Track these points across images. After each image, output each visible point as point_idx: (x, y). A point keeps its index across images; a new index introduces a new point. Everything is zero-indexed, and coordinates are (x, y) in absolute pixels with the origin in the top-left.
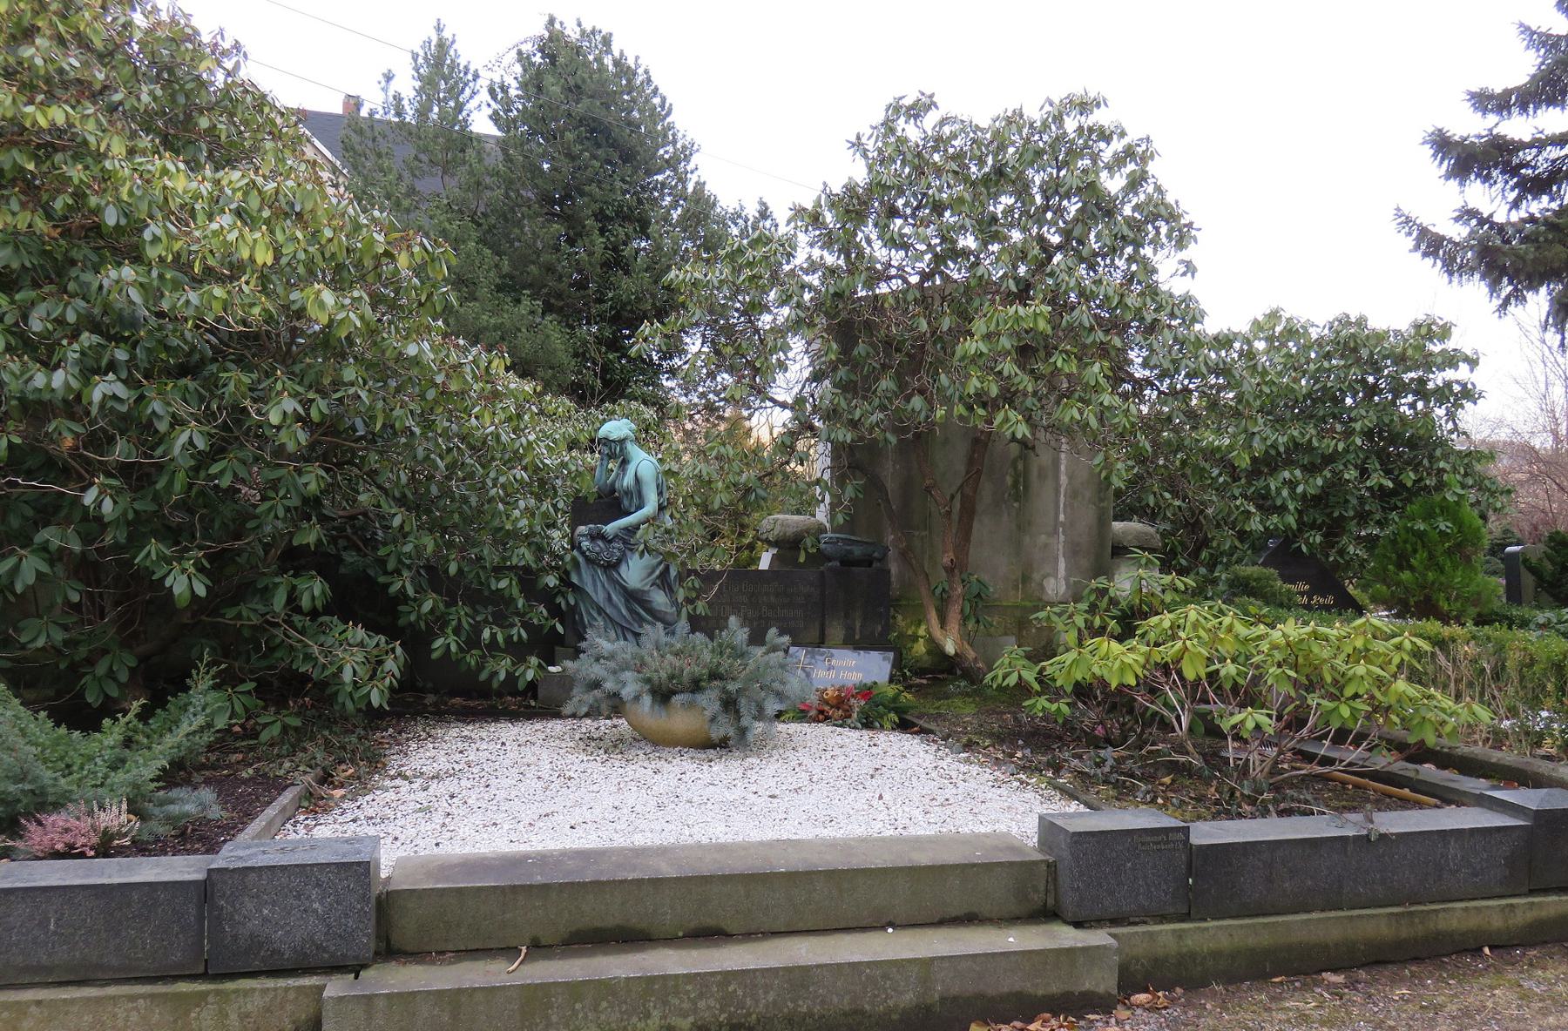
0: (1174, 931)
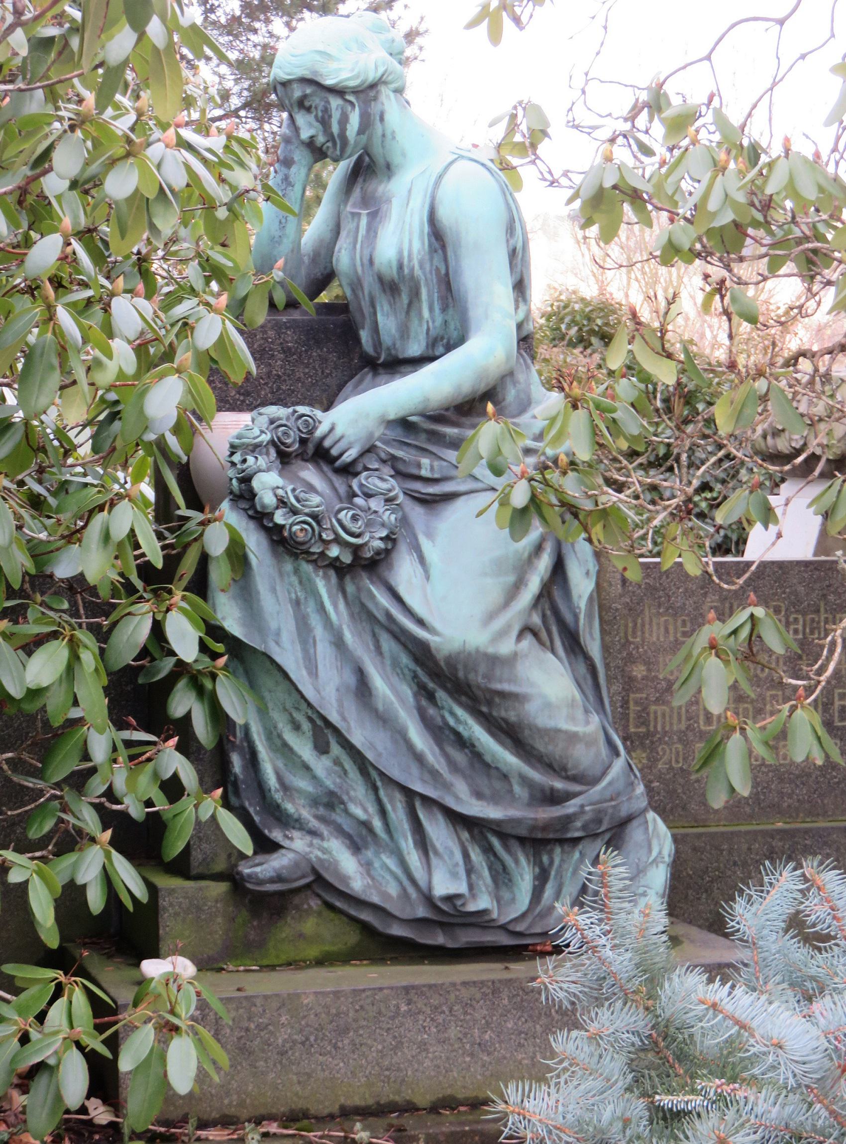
0: (154, 806)
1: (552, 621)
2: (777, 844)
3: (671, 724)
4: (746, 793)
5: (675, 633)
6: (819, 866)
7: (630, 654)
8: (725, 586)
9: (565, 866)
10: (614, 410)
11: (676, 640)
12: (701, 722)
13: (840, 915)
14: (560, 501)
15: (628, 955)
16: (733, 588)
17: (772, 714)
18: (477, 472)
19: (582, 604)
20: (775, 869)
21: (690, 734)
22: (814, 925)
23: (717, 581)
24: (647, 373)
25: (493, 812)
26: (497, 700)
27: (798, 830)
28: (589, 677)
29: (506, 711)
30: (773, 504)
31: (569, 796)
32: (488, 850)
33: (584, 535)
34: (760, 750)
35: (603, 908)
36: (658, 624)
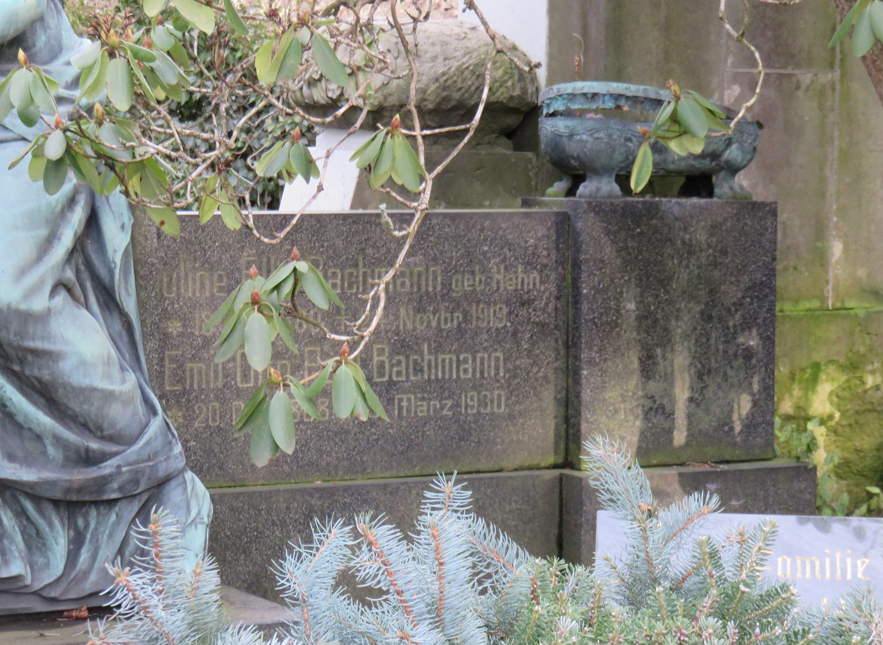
1: (86, 276)
2: (316, 502)
3: (208, 382)
4: (290, 451)
5: (212, 289)
6: (372, 520)
7: (165, 310)
8: (266, 240)
9: (101, 529)
10: (152, 59)
11: (213, 295)
12: (238, 379)
13: (392, 570)
14: (96, 152)
15: (181, 615)
16: (274, 242)
17: (311, 371)
18: (7, 122)
19: (118, 259)
20: (324, 526)
21: (226, 391)
22: (363, 581)
23: (258, 235)
24: (184, 19)
25: (26, 475)
26: (30, 358)
27: (337, 488)
28: (124, 333)
29: (39, 369)
30: (314, 157)
31: (104, 457)
32: (21, 514)
33: (119, 188)
34: (306, 408)
35: (155, 568)
36: (194, 280)
